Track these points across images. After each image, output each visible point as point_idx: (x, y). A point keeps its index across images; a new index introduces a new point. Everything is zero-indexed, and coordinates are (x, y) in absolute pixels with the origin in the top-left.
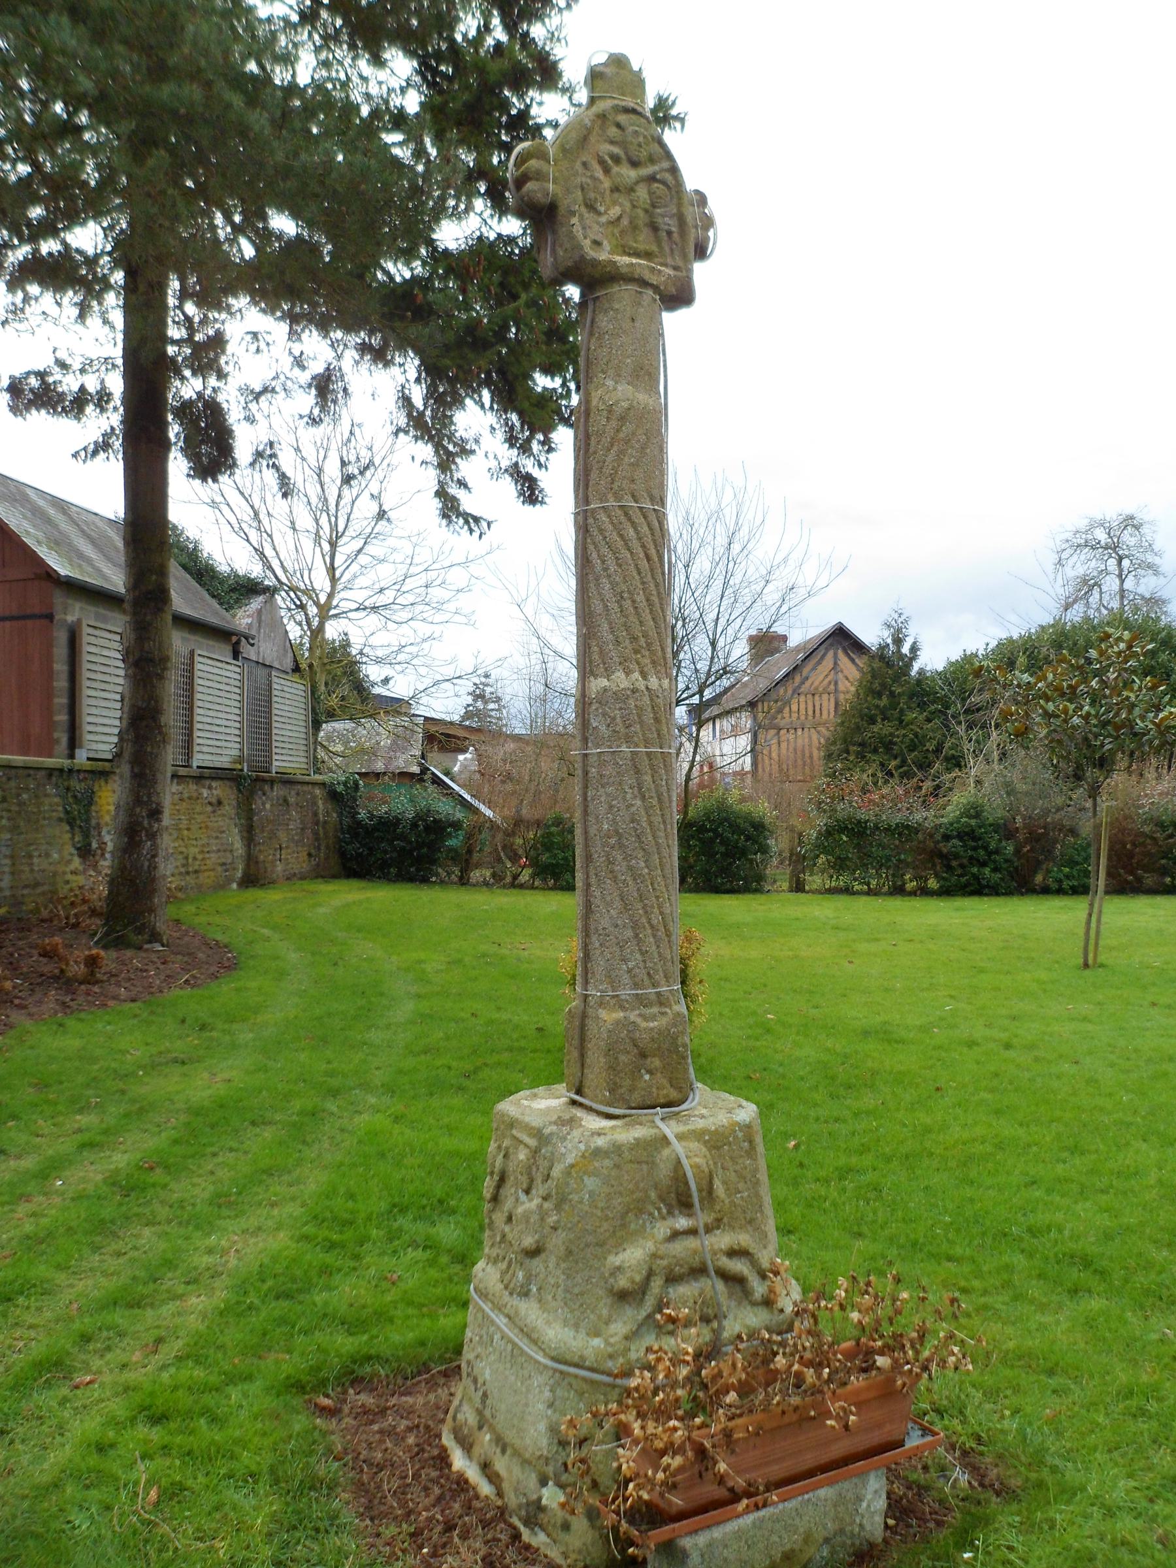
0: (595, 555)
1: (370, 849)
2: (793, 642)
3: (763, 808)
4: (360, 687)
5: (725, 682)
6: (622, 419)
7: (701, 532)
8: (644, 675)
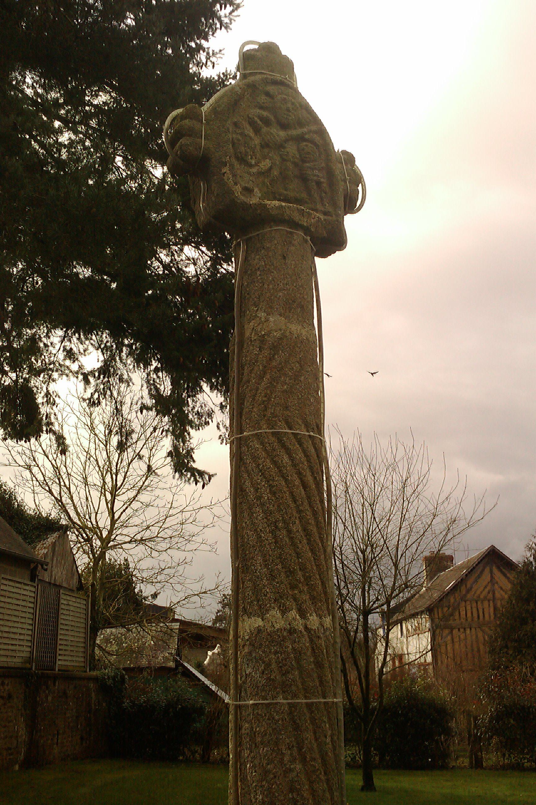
0: (248, 483)
2: (459, 561)
3: (444, 694)
4: (135, 602)
5: (406, 595)
6: (275, 348)
7: (382, 479)
8: (303, 614)
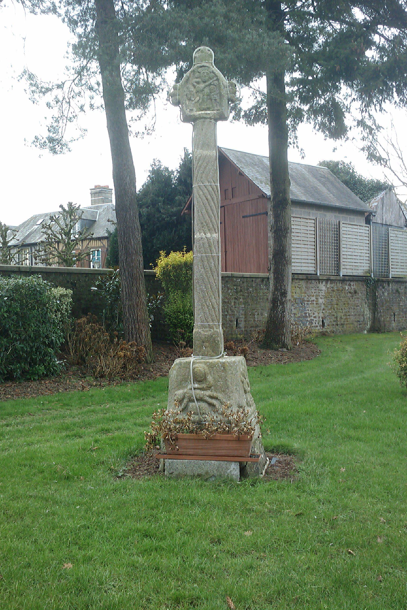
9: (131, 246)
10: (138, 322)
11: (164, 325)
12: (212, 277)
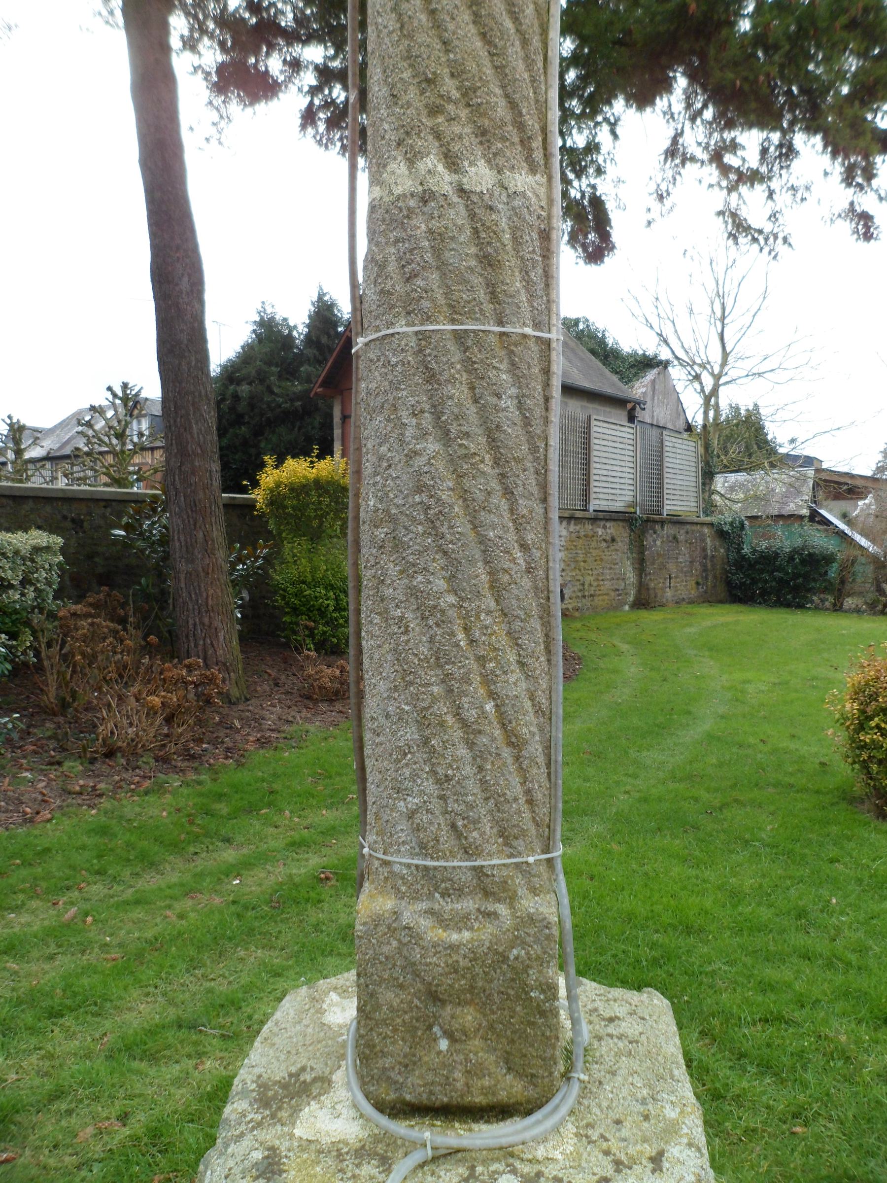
1: (752, 579)
8: (452, 162)
9: (192, 437)
10: (207, 611)
11: (275, 607)
12: (504, 505)
